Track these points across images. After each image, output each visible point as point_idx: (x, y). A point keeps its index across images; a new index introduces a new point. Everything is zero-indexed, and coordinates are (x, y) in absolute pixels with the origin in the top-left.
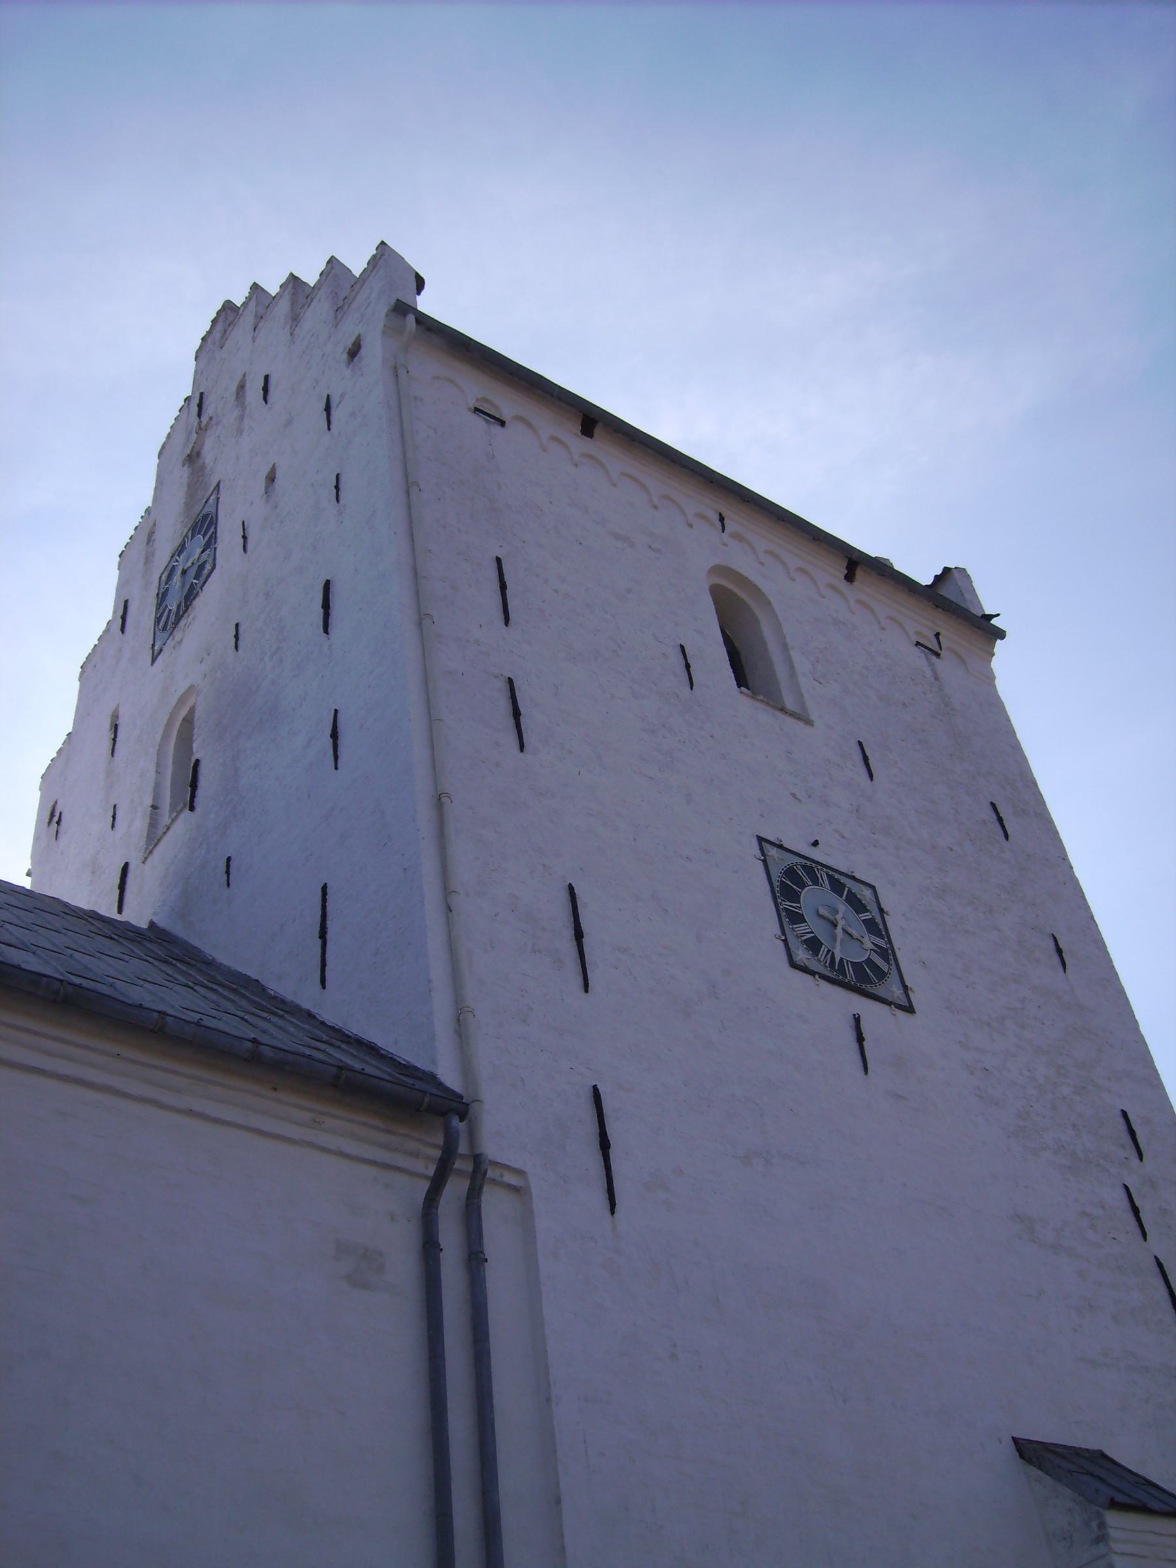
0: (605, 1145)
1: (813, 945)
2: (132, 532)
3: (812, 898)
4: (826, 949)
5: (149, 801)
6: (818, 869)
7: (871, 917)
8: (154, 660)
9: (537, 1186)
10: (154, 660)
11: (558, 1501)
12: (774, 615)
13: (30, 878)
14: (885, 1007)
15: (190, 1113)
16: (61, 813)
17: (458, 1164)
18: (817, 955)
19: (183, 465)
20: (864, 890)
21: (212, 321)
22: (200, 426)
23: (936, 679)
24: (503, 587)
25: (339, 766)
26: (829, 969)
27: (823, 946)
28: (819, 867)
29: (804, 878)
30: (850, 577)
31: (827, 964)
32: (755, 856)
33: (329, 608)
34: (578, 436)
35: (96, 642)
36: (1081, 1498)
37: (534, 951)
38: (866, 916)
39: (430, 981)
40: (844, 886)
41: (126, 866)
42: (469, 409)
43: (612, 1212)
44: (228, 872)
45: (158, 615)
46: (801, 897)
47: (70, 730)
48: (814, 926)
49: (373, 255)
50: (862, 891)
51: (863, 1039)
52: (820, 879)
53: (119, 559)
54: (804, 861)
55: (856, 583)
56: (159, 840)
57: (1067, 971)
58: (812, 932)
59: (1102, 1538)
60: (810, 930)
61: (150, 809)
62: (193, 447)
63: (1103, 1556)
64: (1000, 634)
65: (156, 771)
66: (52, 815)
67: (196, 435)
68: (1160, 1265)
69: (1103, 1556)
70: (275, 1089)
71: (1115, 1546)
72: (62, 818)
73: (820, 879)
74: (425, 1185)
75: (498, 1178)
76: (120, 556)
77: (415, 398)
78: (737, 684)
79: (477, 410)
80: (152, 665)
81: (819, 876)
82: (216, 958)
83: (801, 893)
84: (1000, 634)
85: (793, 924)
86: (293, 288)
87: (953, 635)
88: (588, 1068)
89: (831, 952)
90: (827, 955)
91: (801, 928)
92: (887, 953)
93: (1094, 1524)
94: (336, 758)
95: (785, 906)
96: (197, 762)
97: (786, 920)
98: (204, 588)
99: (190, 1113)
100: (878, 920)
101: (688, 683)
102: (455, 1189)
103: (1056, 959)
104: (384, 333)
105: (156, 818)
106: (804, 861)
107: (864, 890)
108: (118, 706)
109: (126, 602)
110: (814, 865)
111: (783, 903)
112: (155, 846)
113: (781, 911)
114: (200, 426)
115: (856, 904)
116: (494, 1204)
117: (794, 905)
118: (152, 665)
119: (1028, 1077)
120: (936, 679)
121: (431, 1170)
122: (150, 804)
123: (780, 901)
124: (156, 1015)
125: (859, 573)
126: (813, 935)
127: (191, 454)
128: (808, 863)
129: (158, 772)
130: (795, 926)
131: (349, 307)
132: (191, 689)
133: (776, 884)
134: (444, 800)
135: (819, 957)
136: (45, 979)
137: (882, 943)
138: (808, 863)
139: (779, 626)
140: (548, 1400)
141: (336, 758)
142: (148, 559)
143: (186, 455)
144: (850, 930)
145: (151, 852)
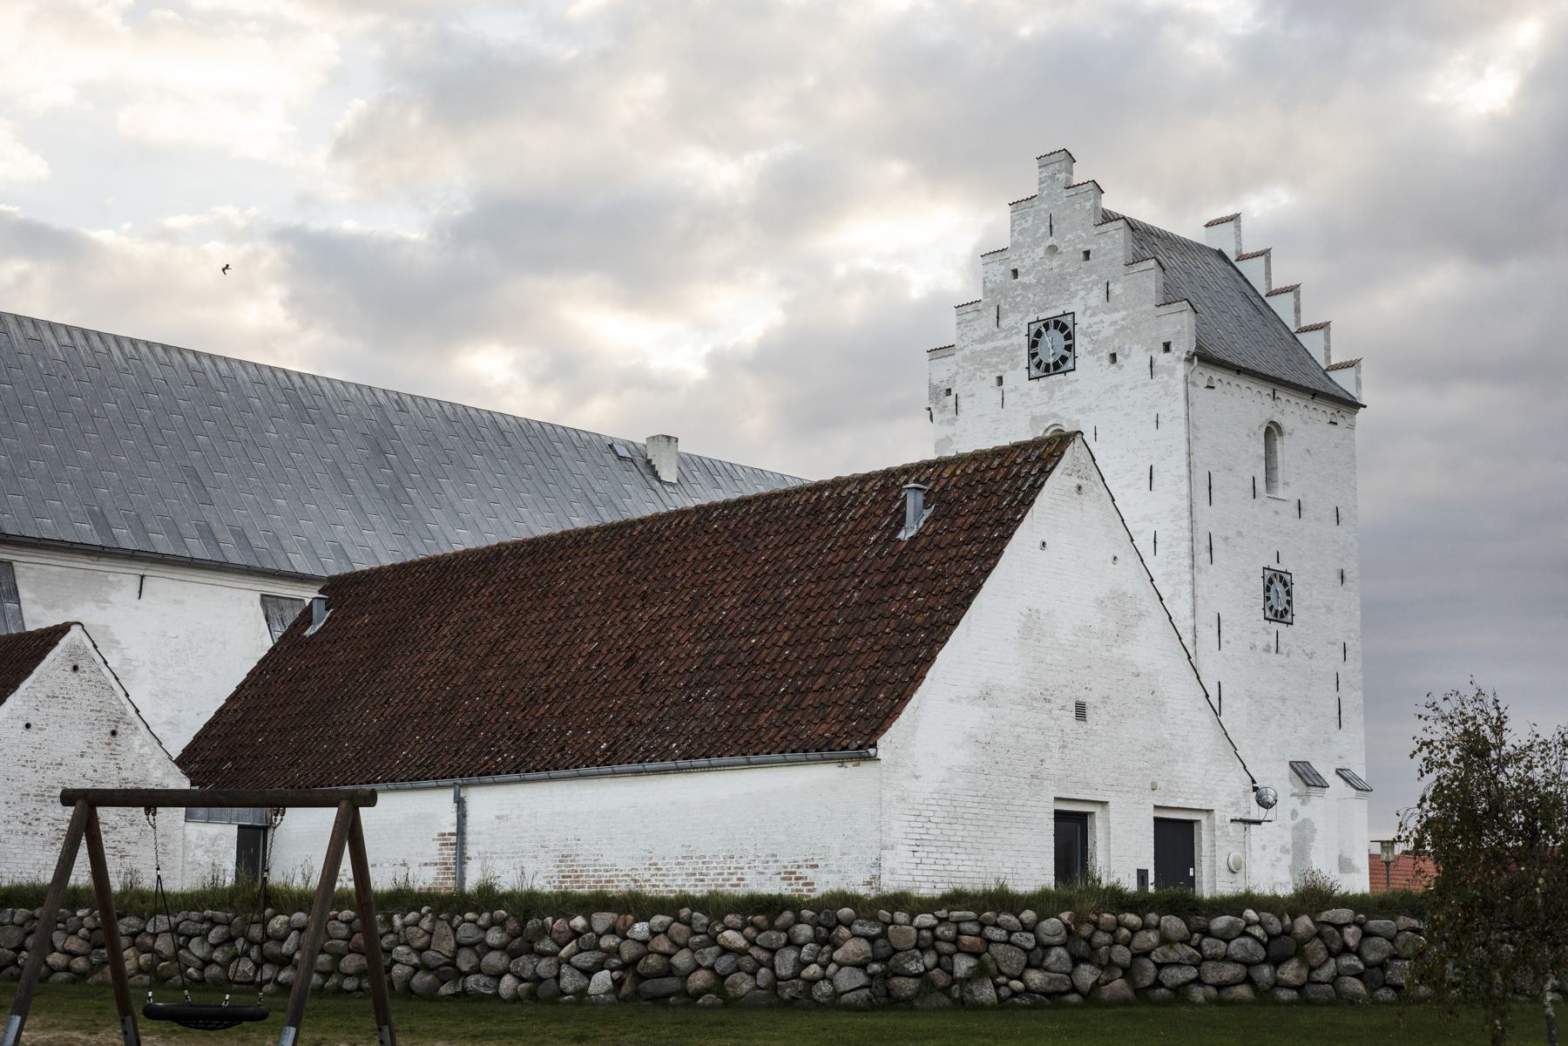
1: (1271, 608)
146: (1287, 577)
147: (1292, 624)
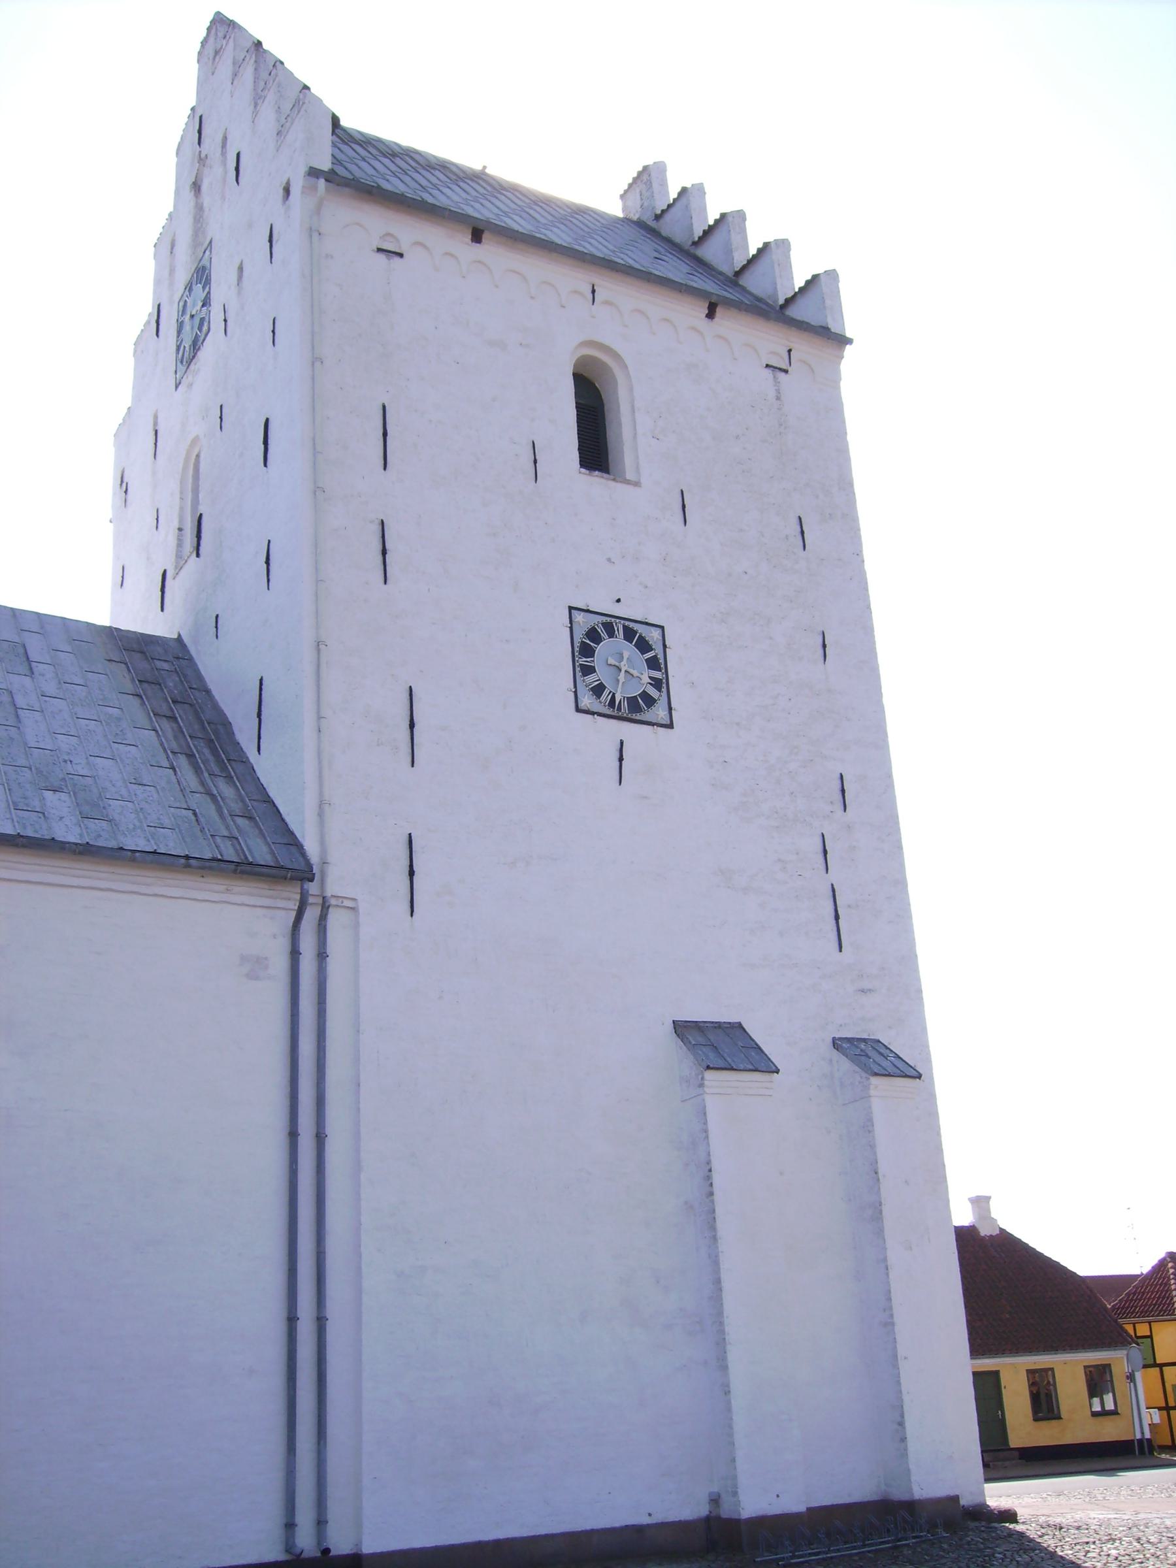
0: (412, 873)
1: (598, 690)
2: (161, 230)
3: (605, 650)
4: (609, 691)
5: (176, 524)
6: (616, 623)
8: (177, 387)
9: (363, 907)
10: (177, 387)
11: (359, 1085)
12: (628, 376)
13: (112, 524)
14: (650, 727)
15: (156, 895)
16: (127, 484)
17: (311, 900)
18: (599, 698)
19: (191, 191)
20: (653, 632)
21: (207, 29)
22: (200, 156)
23: (778, 398)
24: (385, 434)
25: (270, 588)
26: (607, 707)
27: (607, 689)
28: (618, 621)
29: (602, 634)
30: (711, 315)
31: (607, 704)
32: (563, 624)
34: (468, 244)
35: (143, 328)
36: (696, 1062)
37: (378, 745)
39: (304, 783)
40: (635, 632)
41: (165, 572)
42: (373, 250)
43: (412, 915)
44: (216, 627)
45: (179, 343)
46: (596, 652)
47: (193, 104)
48: (602, 674)
50: (652, 633)
51: (623, 760)
52: (616, 632)
53: (154, 248)
54: (605, 619)
55: (716, 319)
56: (181, 568)
57: (826, 662)
58: (599, 680)
59: (701, 1085)
60: (598, 678)
61: (177, 531)
62: (197, 174)
63: (701, 1094)
64: (849, 341)
65: (181, 498)
66: (122, 481)
67: (198, 164)
68: (833, 890)
69: (701, 1094)
70: (203, 877)
71: (707, 1090)
72: (128, 488)
74: (294, 914)
75: (340, 904)
76: (155, 246)
77: (327, 256)
78: (744, 219)
79: (379, 250)
80: (176, 390)
81: (616, 629)
83: (596, 648)
84: (849, 341)
86: (256, 61)
87: (804, 347)
88: (407, 822)
89: (611, 694)
91: (591, 678)
93: (700, 1076)
94: (268, 581)
95: (581, 662)
96: (201, 515)
98: (204, 344)
99: (156, 895)
101: (534, 479)
102: (311, 915)
103: (821, 651)
104: (303, 193)
106: (605, 619)
107: (653, 632)
108: (157, 410)
109: (159, 305)
110: (613, 620)
112: (180, 570)
113: (577, 667)
114: (200, 156)
115: (643, 646)
116: (336, 919)
118: (176, 390)
119: (762, 761)
120: (778, 398)
122: (177, 527)
123: (577, 659)
124: (129, 853)
125: (719, 311)
126: (599, 682)
127: (196, 180)
129: (181, 498)
130: (585, 678)
131: (284, 138)
132: (196, 440)
133: (577, 645)
134: (322, 647)
136: (67, 845)
137: (657, 675)
138: (609, 619)
139: (631, 389)
140: (358, 1031)
141: (268, 581)
142: (171, 284)
143: (191, 183)
144: (631, 671)
145: (177, 574)
146: (653, 636)
147: (670, 726)
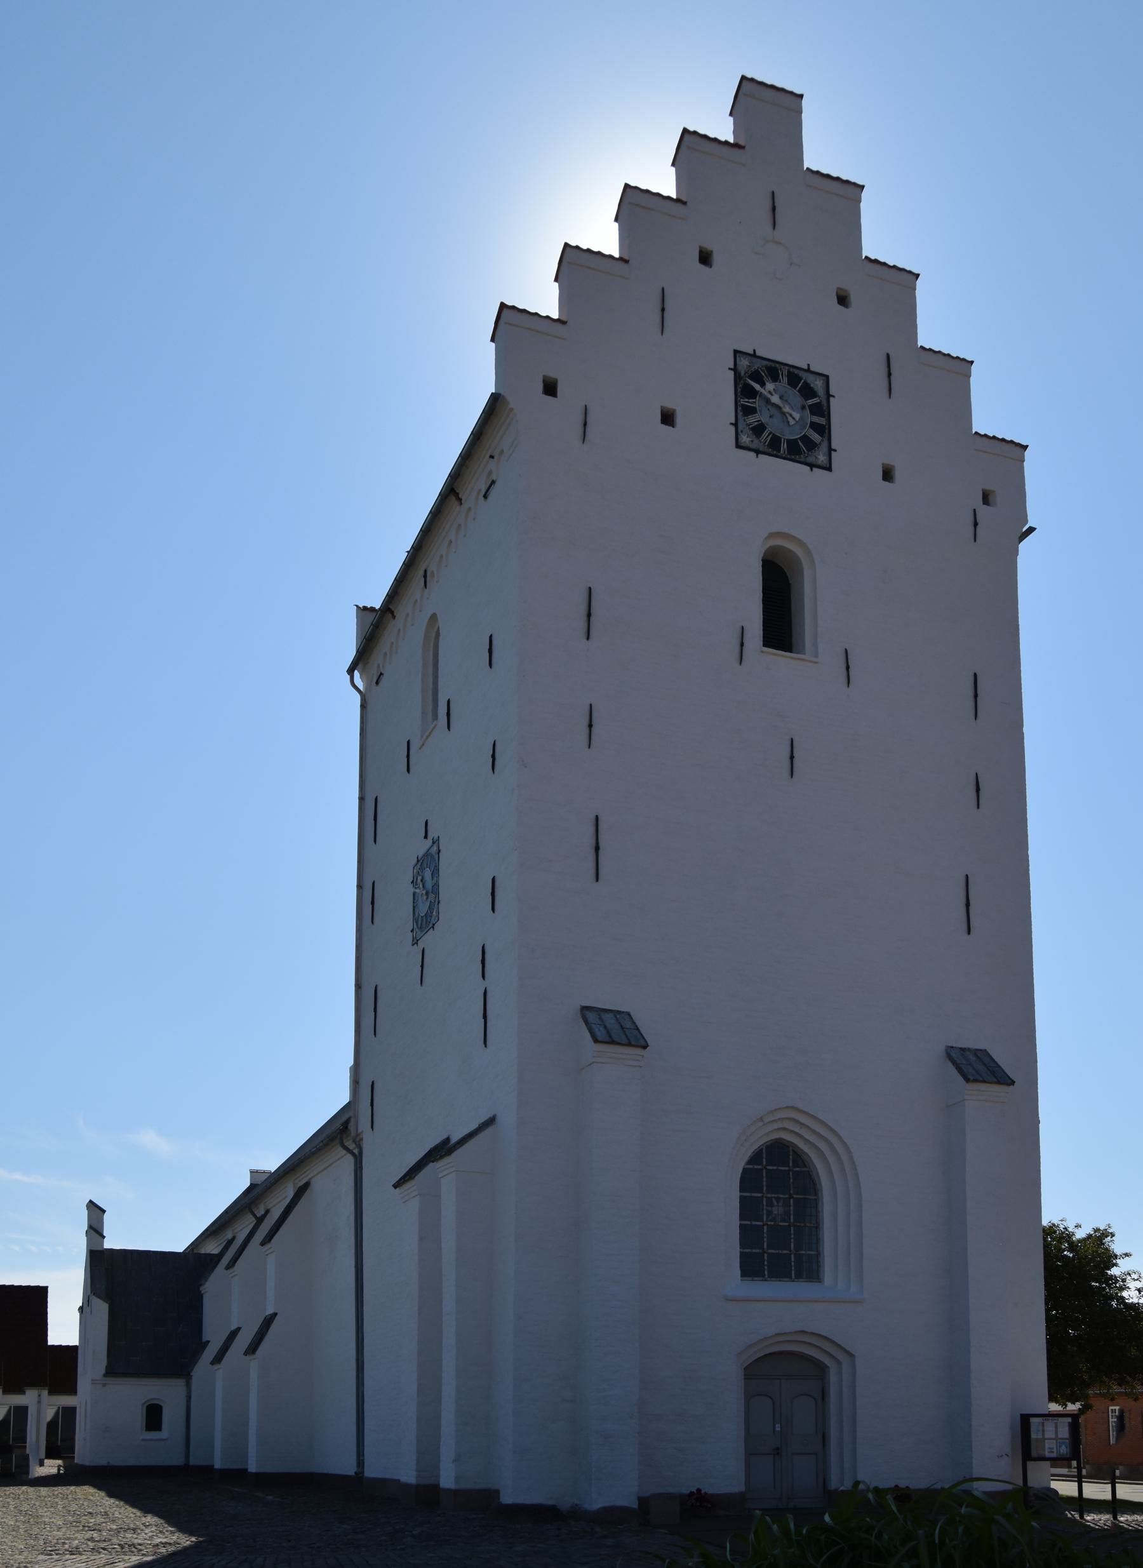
1: (758, 430)
7: (819, 401)
28: (782, 367)
33: (966, 904)
38: (815, 400)
49: (375, 608)
73: (781, 376)
82: (903, 1484)
85: (744, 416)
90: (769, 435)
92: (824, 430)
95: (742, 403)
97: (740, 414)
100: (824, 403)
105: (741, 1250)
111: (742, 400)
117: (750, 401)
121: (1054, 1429)
128: (773, 365)
135: (782, 452)
